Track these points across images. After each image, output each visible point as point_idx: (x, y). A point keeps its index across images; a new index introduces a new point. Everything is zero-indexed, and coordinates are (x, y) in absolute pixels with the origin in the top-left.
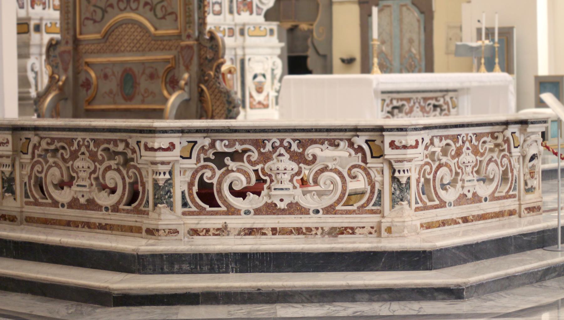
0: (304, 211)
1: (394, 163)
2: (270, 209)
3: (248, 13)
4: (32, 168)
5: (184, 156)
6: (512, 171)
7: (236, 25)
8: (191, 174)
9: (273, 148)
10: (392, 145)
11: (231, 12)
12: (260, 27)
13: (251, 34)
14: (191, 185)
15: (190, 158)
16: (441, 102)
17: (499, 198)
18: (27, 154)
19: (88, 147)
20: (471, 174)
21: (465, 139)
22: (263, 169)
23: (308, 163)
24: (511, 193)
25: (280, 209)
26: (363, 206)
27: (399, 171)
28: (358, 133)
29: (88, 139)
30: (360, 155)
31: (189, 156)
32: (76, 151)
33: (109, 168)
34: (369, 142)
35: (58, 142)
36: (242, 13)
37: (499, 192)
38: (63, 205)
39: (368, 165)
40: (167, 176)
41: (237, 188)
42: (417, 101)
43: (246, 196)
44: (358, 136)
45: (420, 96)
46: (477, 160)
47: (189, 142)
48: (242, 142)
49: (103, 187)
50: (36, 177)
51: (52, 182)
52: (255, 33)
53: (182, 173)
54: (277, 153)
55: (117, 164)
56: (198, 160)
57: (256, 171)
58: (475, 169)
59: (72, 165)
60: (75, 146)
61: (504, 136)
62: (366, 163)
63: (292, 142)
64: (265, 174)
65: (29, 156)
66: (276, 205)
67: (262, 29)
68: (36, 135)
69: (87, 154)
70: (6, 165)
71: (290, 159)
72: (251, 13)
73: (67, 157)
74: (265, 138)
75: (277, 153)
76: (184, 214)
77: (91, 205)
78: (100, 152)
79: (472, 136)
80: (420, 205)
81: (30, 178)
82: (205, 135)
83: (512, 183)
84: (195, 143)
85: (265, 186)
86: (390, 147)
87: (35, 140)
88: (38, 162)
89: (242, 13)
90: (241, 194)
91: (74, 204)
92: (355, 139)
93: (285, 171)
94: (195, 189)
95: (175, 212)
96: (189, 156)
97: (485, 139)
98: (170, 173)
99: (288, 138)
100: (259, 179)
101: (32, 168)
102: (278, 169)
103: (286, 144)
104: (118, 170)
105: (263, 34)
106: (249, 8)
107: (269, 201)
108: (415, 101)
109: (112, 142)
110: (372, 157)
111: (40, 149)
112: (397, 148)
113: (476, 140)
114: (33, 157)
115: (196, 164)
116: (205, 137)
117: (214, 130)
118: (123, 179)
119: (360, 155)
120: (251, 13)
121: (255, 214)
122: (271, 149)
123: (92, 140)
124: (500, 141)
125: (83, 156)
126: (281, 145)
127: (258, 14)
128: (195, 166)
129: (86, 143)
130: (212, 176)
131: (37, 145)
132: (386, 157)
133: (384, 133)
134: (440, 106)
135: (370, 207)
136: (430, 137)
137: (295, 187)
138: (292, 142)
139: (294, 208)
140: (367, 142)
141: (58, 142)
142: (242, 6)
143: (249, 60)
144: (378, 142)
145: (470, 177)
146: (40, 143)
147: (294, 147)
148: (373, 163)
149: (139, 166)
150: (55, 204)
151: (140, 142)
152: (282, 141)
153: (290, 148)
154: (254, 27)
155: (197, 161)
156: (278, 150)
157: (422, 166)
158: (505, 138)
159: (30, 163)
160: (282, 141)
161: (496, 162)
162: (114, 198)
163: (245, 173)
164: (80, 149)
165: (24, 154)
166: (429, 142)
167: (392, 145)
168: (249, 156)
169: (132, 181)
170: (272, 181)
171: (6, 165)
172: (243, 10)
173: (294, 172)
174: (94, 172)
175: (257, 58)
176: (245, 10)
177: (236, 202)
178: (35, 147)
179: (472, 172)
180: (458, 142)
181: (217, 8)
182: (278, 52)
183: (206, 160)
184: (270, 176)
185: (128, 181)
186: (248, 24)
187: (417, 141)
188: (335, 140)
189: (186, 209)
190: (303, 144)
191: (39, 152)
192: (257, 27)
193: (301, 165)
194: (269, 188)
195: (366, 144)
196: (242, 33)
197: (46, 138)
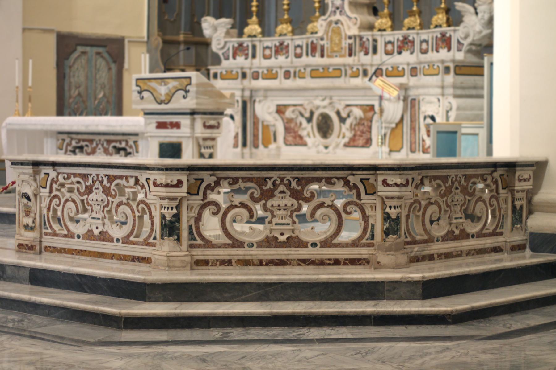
1: (385, 200)
3: (446, 50)
4: (51, 201)
5: (192, 193)
6: (500, 211)
7: (372, 65)
10: (385, 182)
11: (307, 55)
12: (434, 65)
13: (425, 73)
15: (198, 194)
17: (485, 235)
18: (46, 188)
19: (102, 182)
20: (460, 212)
21: (454, 179)
23: (307, 200)
24: (498, 230)
25: (280, 242)
27: (390, 207)
28: (354, 172)
29: (102, 175)
30: (354, 191)
31: (196, 193)
32: (92, 186)
34: (364, 181)
35: (74, 177)
36: (441, 50)
37: (487, 229)
38: (79, 237)
39: (362, 201)
40: (175, 211)
42: (100, 143)
44: (353, 175)
45: (103, 138)
46: (465, 199)
47: (196, 179)
48: (84, 140)
50: (54, 208)
52: (429, 72)
53: (189, 209)
54: (279, 190)
55: (127, 199)
58: (463, 208)
59: (87, 199)
60: (90, 182)
61: (493, 178)
63: (291, 180)
65: (200, 197)
67: (435, 67)
68: (54, 170)
69: (101, 189)
70: (165, 207)
71: (290, 196)
72: (246, 59)
73: (82, 191)
77: (104, 237)
78: (113, 187)
79: (461, 176)
80: (409, 239)
81: (49, 209)
82: (211, 173)
83: (499, 221)
84: (202, 180)
86: (383, 184)
87: (53, 174)
88: (56, 196)
89: (441, 50)
91: (89, 236)
92: (350, 178)
93: (286, 208)
95: (181, 245)
96: (196, 193)
97: (474, 180)
98: (177, 207)
99: (288, 175)
101: (51, 201)
103: (286, 182)
104: (128, 204)
105: (436, 72)
106: (447, 44)
108: (98, 142)
109: (124, 178)
110: (367, 194)
111: (58, 183)
112: (388, 185)
113: (465, 181)
114: (51, 192)
115: (202, 200)
116: (211, 175)
117: (237, 168)
118: (133, 212)
119: (354, 191)
120: (246, 59)
122: (272, 187)
123: (294, 178)
124: (489, 181)
125: (97, 191)
127: (459, 50)
128: (201, 202)
130: (217, 211)
131: (55, 179)
132: (379, 193)
133: (378, 172)
135: (364, 241)
136: (420, 177)
137: (294, 223)
138: (291, 180)
140: (362, 180)
141: (74, 177)
142: (440, 43)
144: (372, 181)
145: (459, 215)
146: (57, 177)
147: (294, 184)
148: (366, 200)
149: (148, 201)
150: (69, 235)
151: (149, 179)
152: (282, 179)
153: (290, 185)
154: (429, 66)
155: (203, 197)
156: (279, 188)
157: (411, 204)
158: (494, 180)
159: (49, 196)
160: (282, 179)
161: (484, 202)
164: (94, 185)
165: (43, 188)
166: (419, 182)
167: (385, 182)
169: (140, 214)
171: (165, 207)
172: (442, 48)
173: (293, 208)
174: (107, 205)
175: (428, 98)
176: (443, 46)
178: (53, 181)
179: (460, 211)
180: (447, 182)
185: (137, 214)
186: (401, 64)
187: (407, 181)
188: (331, 178)
190: (304, 182)
192: (431, 65)
193: (300, 201)
195: (361, 183)
197: (64, 173)
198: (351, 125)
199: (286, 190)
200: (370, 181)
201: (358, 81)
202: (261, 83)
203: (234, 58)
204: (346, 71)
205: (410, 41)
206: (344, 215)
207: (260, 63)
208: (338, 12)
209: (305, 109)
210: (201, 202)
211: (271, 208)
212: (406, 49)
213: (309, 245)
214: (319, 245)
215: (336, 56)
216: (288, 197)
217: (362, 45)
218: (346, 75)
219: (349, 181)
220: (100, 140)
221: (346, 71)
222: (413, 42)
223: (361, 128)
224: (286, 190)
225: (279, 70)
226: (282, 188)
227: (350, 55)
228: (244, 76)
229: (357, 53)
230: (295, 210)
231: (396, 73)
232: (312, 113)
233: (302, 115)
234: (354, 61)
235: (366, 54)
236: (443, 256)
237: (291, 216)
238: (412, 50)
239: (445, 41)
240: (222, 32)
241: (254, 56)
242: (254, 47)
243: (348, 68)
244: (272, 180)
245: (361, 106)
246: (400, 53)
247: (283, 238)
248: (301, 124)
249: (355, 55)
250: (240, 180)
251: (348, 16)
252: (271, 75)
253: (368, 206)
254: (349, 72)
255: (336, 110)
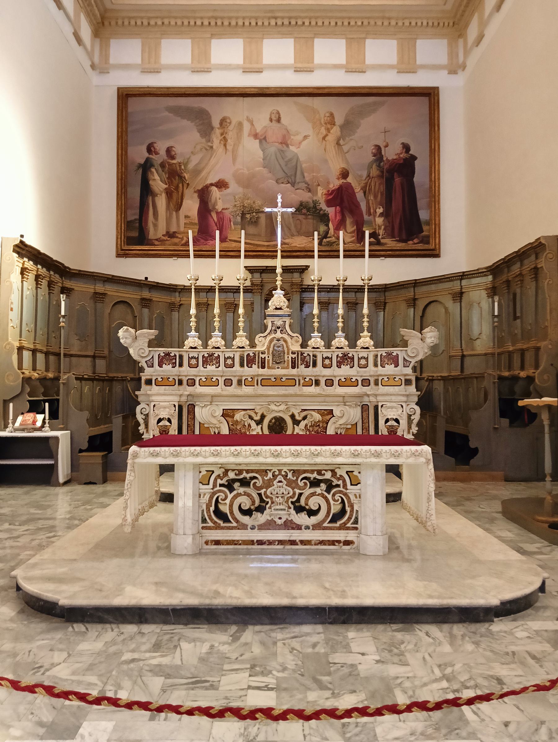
0: (299, 527)
2: (269, 525)
7: (335, 377)
8: (209, 496)
9: (273, 476)
11: (376, 365)
14: (208, 506)
15: (208, 484)
16: (328, 475)
22: (265, 492)
26: (345, 524)
33: (313, 494)
41: (245, 507)
43: (252, 514)
47: (207, 471)
49: (299, 509)
51: (240, 505)
52: (346, 384)
54: (277, 480)
56: (215, 486)
57: (260, 495)
62: (347, 489)
63: (288, 472)
64: (267, 497)
66: (275, 522)
74: (267, 468)
75: (277, 480)
76: (203, 528)
84: (213, 472)
85: (268, 506)
90: (248, 513)
94: (212, 509)
100: (262, 500)
102: (277, 494)
107: (270, 519)
110: (351, 485)
120: (397, 366)
121: (313, 529)
123: (290, 470)
126: (280, 474)
128: (212, 491)
129: (283, 473)
134: (326, 481)
138: (288, 472)
139: (289, 525)
143: (382, 406)
147: (290, 476)
152: (280, 471)
153: (287, 476)
156: (278, 478)
162: (314, 520)
163: (249, 495)
168: (255, 483)
170: (272, 503)
173: (289, 495)
177: (245, 519)
181: (363, 362)
182: (416, 399)
183: (221, 485)
184: (271, 498)
188: (321, 470)
189: (204, 525)
191: (222, 482)
194: (270, 508)
196: (376, 383)
198: (306, 425)
199: (283, 480)
200: (354, 473)
201: (312, 389)
202: (198, 389)
203: (160, 365)
204: (299, 380)
205: (349, 358)
206: (332, 502)
207: (186, 371)
208: (279, 331)
209: (256, 413)
210: (212, 491)
211: (271, 496)
212: (345, 364)
213: (303, 527)
214: (311, 528)
215: (278, 368)
216: (284, 486)
217: (303, 360)
218: (299, 384)
219: (336, 473)
220: (280, 471)
221: (299, 380)
222: (352, 359)
223: (316, 429)
224: (283, 480)
225: (219, 378)
226: (280, 478)
227: (293, 367)
228: (180, 383)
229: (299, 366)
230: (291, 497)
231: (349, 383)
232: (263, 417)
233: (251, 417)
234: (298, 372)
235: (307, 366)
236: (313, 543)
237: (287, 502)
238: (352, 365)
239: (392, 359)
240: (143, 343)
241: (181, 365)
242: (181, 357)
243: (301, 378)
244: (272, 471)
245: (318, 411)
246: (339, 366)
247: (279, 522)
248: (249, 425)
249: (298, 368)
250: (244, 472)
251: (288, 334)
252: (210, 382)
253: (353, 494)
254: (302, 381)
255: (290, 414)
